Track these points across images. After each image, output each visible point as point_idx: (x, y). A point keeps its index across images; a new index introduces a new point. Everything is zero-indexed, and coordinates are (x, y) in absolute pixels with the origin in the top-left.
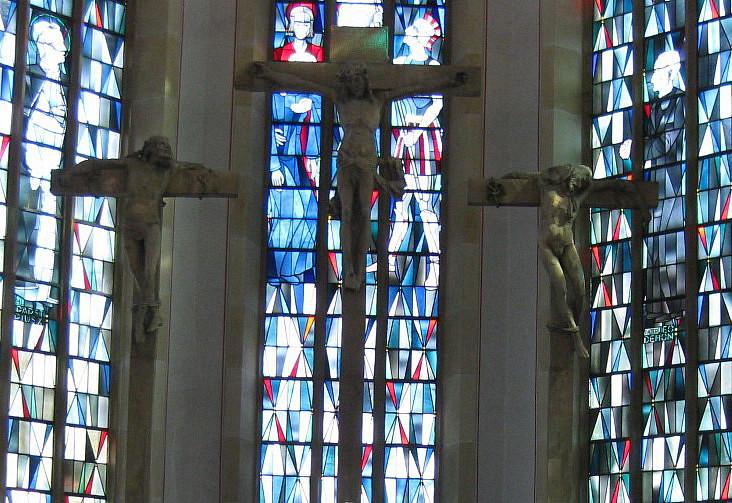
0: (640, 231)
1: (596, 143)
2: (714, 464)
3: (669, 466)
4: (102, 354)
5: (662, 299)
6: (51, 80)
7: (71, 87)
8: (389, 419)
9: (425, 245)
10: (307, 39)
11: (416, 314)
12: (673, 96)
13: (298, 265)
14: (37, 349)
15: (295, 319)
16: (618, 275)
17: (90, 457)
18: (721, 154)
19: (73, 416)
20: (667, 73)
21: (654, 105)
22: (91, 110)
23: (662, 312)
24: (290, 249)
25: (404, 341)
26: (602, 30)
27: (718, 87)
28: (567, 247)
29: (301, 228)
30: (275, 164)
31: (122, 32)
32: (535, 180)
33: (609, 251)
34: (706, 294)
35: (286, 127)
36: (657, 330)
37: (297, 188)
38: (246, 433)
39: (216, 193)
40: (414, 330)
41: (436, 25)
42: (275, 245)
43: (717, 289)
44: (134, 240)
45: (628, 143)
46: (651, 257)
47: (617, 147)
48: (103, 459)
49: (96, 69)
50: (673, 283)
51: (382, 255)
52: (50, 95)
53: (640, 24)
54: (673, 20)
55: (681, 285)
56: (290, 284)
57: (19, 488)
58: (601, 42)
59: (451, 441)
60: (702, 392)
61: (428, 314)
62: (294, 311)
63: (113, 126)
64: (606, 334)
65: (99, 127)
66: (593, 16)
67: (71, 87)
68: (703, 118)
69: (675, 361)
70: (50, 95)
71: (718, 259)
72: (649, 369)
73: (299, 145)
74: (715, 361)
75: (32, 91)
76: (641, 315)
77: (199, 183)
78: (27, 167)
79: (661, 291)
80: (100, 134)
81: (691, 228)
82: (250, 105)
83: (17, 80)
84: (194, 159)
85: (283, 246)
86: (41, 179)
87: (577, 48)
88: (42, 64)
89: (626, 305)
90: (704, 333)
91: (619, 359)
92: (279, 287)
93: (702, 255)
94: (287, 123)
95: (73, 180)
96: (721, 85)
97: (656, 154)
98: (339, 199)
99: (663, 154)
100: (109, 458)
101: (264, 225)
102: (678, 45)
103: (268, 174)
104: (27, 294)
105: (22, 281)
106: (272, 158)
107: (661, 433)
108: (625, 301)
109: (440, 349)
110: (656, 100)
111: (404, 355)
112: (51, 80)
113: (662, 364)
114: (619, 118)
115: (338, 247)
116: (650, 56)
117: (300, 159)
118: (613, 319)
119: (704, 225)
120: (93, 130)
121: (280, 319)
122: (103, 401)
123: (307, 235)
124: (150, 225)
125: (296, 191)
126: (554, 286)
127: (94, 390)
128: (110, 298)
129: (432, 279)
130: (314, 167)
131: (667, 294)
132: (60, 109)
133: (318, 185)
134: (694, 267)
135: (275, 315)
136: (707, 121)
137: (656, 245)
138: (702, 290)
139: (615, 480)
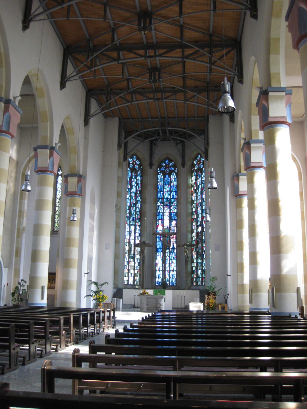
1: (193, 236)
2: (204, 273)
3: (200, 273)
4: (139, 261)
5: (199, 255)
7: (135, 232)
8: (171, 268)
9: (174, 248)
10: (161, 224)
11: (174, 255)
12: (200, 232)
14: (132, 262)
16: (195, 252)
17: (138, 273)
19: (136, 269)
20: (200, 229)
22: (137, 235)
24: (159, 248)
25: (172, 259)
28: (187, 252)
30: (157, 239)
32: (183, 244)
33: (194, 249)
38: (154, 269)
39: (150, 246)
40: (173, 257)
43: (205, 254)
44: (142, 252)
48: (139, 273)
49: (137, 230)
50: (200, 253)
51: (169, 248)
52: (133, 234)
53: (197, 223)
55: (201, 253)
59: (177, 270)
60: (203, 265)
61: (175, 255)
63: (139, 236)
64: (194, 258)
67: (135, 232)
68: (203, 235)
75: (131, 234)
76: (197, 257)
77: (149, 245)
80: (138, 237)
82: (166, 126)
83: (129, 233)
84: (148, 243)
91: (195, 261)
95: (136, 245)
98: (194, 159)
101: (156, 246)
102: (201, 226)
103: (157, 240)
104: (131, 256)
105: (130, 254)
107: (199, 270)
109: (176, 259)
111: (172, 260)
114: (195, 234)
118: (195, 256)
120: (137, 237)
122: (139, 266)
126: (185, 255)
127: (138, 265)
128: (139, 255)
129: (175, 251)
132: (134, 235)
134: (202, 251)
135: (158, 256)
139: (195, 274)
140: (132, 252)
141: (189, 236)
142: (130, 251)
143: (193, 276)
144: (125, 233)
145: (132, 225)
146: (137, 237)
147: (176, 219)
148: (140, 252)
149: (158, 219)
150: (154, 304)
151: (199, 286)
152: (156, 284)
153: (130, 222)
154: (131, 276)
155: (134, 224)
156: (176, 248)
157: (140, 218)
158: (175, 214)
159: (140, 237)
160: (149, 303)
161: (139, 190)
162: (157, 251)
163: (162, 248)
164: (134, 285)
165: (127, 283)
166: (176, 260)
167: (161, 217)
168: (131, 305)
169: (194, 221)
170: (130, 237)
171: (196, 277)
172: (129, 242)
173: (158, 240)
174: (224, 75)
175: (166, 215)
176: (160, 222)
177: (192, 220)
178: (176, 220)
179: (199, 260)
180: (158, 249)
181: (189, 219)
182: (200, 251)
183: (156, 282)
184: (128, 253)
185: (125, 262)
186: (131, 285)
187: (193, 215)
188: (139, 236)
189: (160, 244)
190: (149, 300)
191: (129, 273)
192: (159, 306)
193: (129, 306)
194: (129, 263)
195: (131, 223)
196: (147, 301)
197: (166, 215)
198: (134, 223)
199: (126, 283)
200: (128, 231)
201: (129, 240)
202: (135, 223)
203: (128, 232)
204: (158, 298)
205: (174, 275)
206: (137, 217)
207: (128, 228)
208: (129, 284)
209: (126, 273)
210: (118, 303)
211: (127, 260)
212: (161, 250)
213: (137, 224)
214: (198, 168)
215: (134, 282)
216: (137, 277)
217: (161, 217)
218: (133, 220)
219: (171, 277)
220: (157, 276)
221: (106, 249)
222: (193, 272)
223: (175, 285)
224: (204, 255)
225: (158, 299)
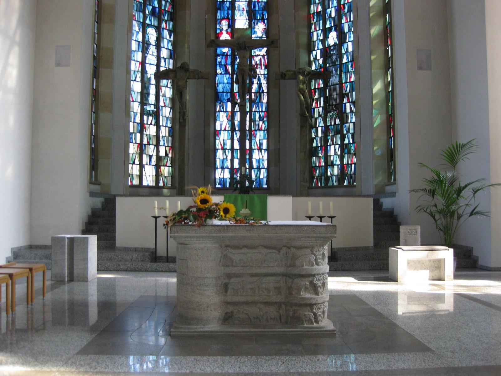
1: (312, 59)
4: (169, 125)
5: (333, 105)
6: (153, 45)
7: (158, 47)
10: (227, 30)
12: (335, 45)
13: (225, 97)
14: (151, 124)
15: (225, 113)
17: (167, 155)
18: (349, 62)
19: (161, 143)
20: (333, 38)
22: (164, 53)
23: (333, 109)
24: (223, 92)
25: (257, 118)
27: (348, 42)
28: (304, 91)
29: (226, 86)
30: (218, 67)
37: (225, 74)
38: (212, 147)
39: (202, 78)
40: (260, 116)
43: (349, 102)
44: (179, 93)
45: (322, 59)
47: (318, 60)
48: (170, 155)
50: (336, 100)
52: (152, 49)
53: (324, 24)
55: (338, 101)
58: (313, 29)
59: (272, 148)
60: (345, 132)
62: (225, 110)
63: (171, 58)
64: (316, 115)
67: (158, 47)
68: (343, 52)
69: (337, 123)
70: (152, 49)
74: (348, 123)
75: (147, 49)
76: (326, 110)
77: (197, 75)
79: (332, 103)
80: (167, 60)
81: (341, 84)
92: (220, 104)
93: (344, 92)
95: (159, 75)
101: (215, 86)
102: (336, 30)
103: (216, 70)
105: (146, 104)
106: (217, 66)
109: (267, 121)
110: (329, 46)
111: (257, 123)
112: (153, 45)
113: (333, 124)
114: (319, 52)
116: (327, 33)
117: (225, 66)
118: (318, 110)
119: (344, 83)
120: (165, 59)
121: (221, 113)
122: (170, 138)
123: (228, 87)
124: (183, 88)
125: (224, 75)
127: (167, 135)
128: (171, 108)
129: (265, 100)
130: (229, 68)
132: (155, 54)
134: (342, 96)
135: (219, 112)
137: (330, 88)
138: (344, 102)
139: (320, 158)
140: (152, 99)
141: (303, 58)
142: (144, 94)
143: (315, 163)
144: (129, 45)
145: (150, 26)
146: (165, 59)
147: (266, 17)
148: (172, 100)
149: (219, 17)
150: (271, 282)
151: (333, 187)
152: (215, 184)
153: (145, 18)
154: (148, 164)
155: (156, 24)
156: (268, 93)
157: (171, 13)
158: (264, 6)
159: (171, 61)
160: (237, 276)
161: (168, 11)
162: (217, 97)
163: (230, 93)
164: (157, 186)
165: (138, 183)
166: (266, 122)
167: (226, 12)
168: (147, 250)
169: (315, 20)
170: (144, 58)
171: (323, 164)
172: (143, 71)
173: (219, 71)
175: (241, 9)
176: (224, 24)
177: (309, 17)
178: (266, 21)
179: (331, 119)
180: (220, 94)
181: (304, 13)
182: (335, 96)
183: (215, 179)
184: (139, 100)
185: (131, 124)
186: (148, 187)
187: (312, 6)
188: (171, 58)
189: (225, 81)
190: (236, 256)
191: (144, 156)
192: (306, 295)
193: (135, 255)
194: (142, 127)
195: (148, 21)
196: (226, 261)
197: (241, 9)
198: (155, 23)
199: (136, 182)
200: (140, 39)
201: (143, 64)
202: (160, 23)
203: (139, 42)
204: (298, 243)
205: (263, 160)
206: (163, 8)
207: (140, 34)
208: (145, 183)
209: (134, 155)
210: (75, 257)
211: (138, 120)
213: (164, 24)
215: (157, 181)
216: (166, 166)
217: (228, 12)
218: (153, 13)
219: (255, 165)
220: (218, 164)
221: (58, 65)
222: (313, 152)
223: (265, 186)
225: (301, 248)
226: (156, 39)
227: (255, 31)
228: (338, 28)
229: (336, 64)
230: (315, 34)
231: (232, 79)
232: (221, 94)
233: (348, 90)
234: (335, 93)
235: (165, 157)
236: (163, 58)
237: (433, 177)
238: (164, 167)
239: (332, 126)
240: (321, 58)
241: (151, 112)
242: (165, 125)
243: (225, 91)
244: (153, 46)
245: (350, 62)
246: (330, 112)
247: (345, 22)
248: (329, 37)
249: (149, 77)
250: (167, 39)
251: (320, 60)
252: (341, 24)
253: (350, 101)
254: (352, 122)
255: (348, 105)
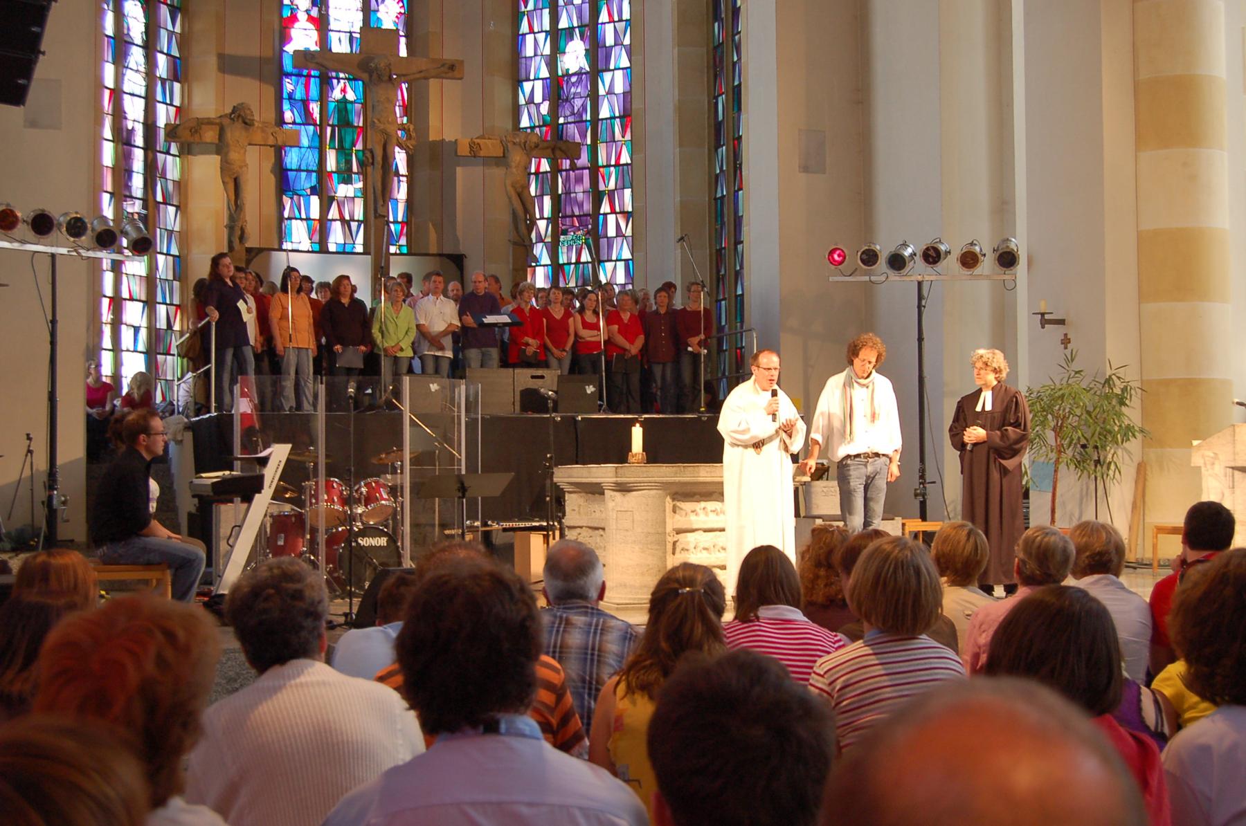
0: (556, 169)
1: (522, 101)
4: (175, 251)
5: (573, 216)
6: (137, 45)
7: (150, 47)
10: (307, 11)
12: (579, 74)
13: (305, 182)
15: (305, 222)
17: (170, 326)
18: (615, 118)
20: (575, 57)
21: (566, 78)
23: (573, 226)
24: (299, 170)
26: (526, 17)
27: (613, 70)
29: (307, 154)
31: (179, 6)
34: (605, 215)
35: (293, 78)
36: (569, 237)
37: (304, 124)
41: (401, 4)
42: (289, 167)
43: (613, 211)
45: (547, 104)
46: (564, 185)
47: (538, 106)
50: (581, 206)
52: (136, 56)
53: (555, 19)
54: (580, 17)
56: (300, 196)
57: (128, 350)
58: (524, 27)
61: (400, 219)
62: (304, 216)
65: (167, 79)
66: (518, 7)
69: (583, 259)
70: (136, 56)
71: (613, 191)
72: (564, 264)
73: (304, 92)
74: (611, 261)
78: (125, 113)
79: (572, 211)
81: (594, 169)
85: (294, 167)
86: (134, 121)
87: (507, 31)
88: (131, 34)
89: (547, 219)
90: (603, 242)
92: (292, 198)
93: (602, 187)
94: (294, 75)
96: (615, 69)
97: (568, 113)
99: (573, 114)
100: (182, 326)
103: (281, 113)
106: (284, 101)
108: (546, 215)
110: (568, 75)
112: (137, 45)
113: (574, 260)
114: (539, 85)
115: (334, 169)
116: (562, 43)
117: (306, 103)
119: (603, 167)
121: (294, 221)
123: (311, 159)
124: (241, 167)
125: (303, 127)
127: (171, 277)
130: (315, 108)
131: (577, 213)
133: (318, 123)
134: (597, 197)
135: (289, 219)
136: (604, 93)
137: (568, 178)
138: (602, 212)
140: (137, 182)
142: (123, 171)
146: (163, 81)
174: (437, 464)
212: (309, 177)
214: (310, 553)
216: (168, 353)
224: (605, 221)
226: (144, 30)
227: (378, 18)
228: (591, 32)
229: (584, 119)
230: (530, 39)
231: (321, 137)
232: (294, 173)
233: (612, 185)
234: (579, 189)
235: (166, 330)
236: (160, 78)
237: (1077, 352)
238: (164, 357)
239: (573, 266)
240: (544, 100)
241: (136, 217)
242: (165, 251)
243: (303, 167)
244: (138, 48)
245: (617, 117)
246: (565, 233)
247: (608, 21)
248: (567, 50)
249: (130, 128)
250: (167, 29)
251: (542, 105)
252: (598, 24)
253: (617, 209)
254: (621, 260)
255: (611, 219)
